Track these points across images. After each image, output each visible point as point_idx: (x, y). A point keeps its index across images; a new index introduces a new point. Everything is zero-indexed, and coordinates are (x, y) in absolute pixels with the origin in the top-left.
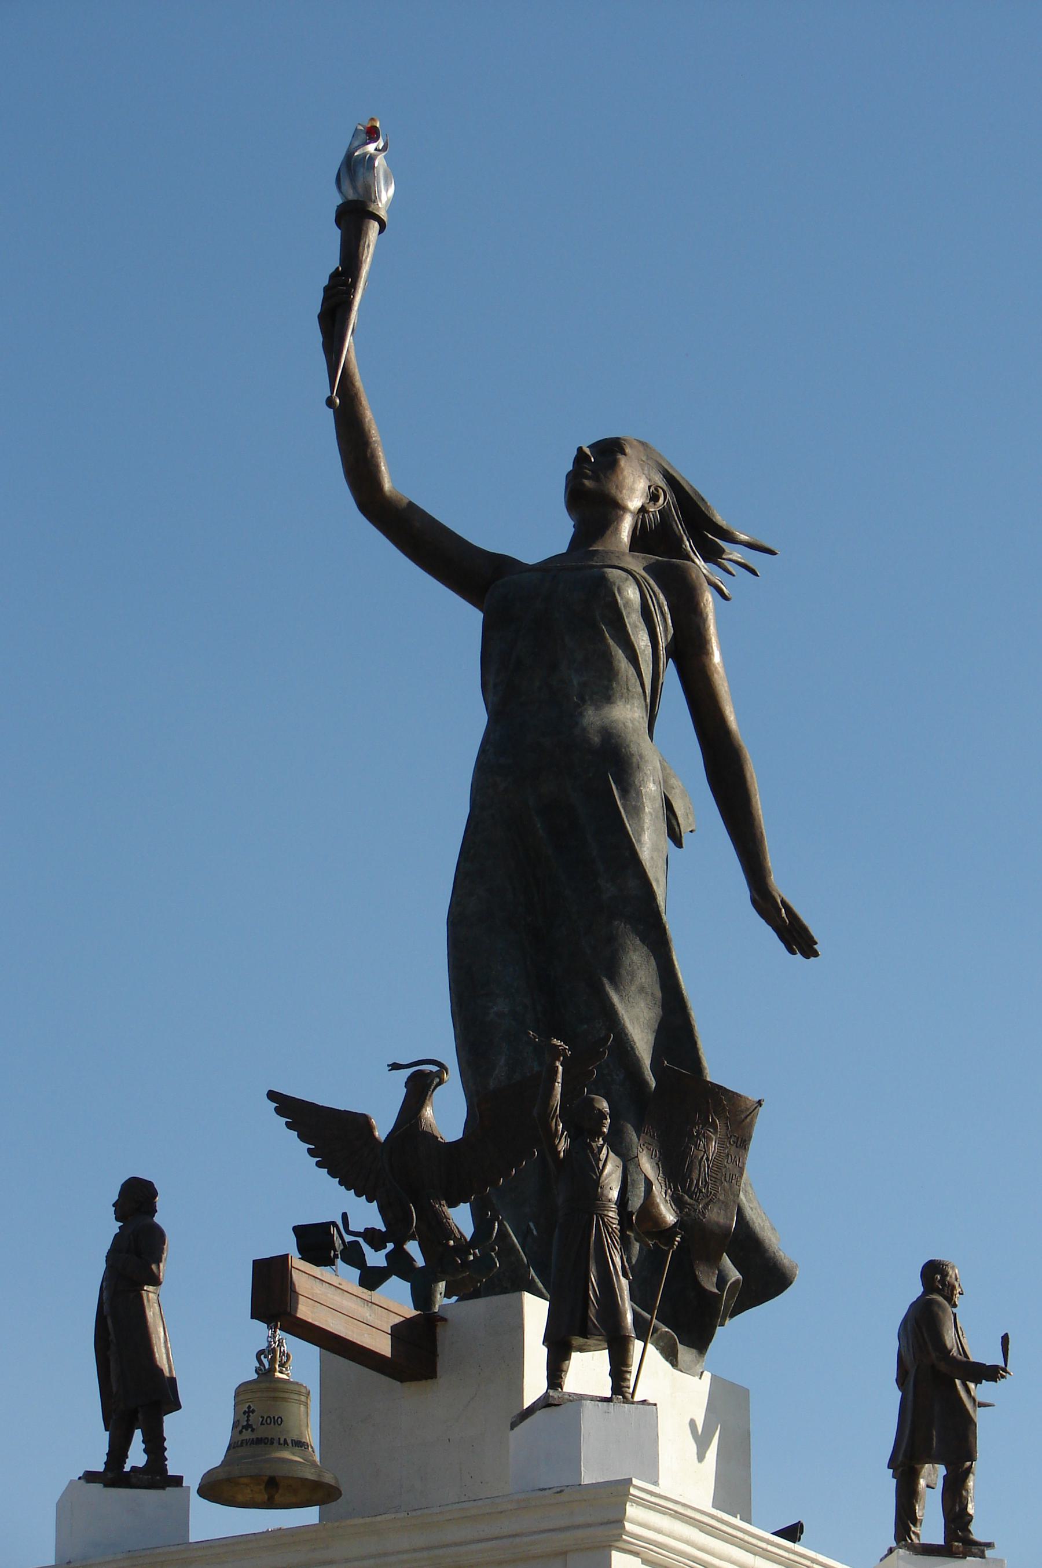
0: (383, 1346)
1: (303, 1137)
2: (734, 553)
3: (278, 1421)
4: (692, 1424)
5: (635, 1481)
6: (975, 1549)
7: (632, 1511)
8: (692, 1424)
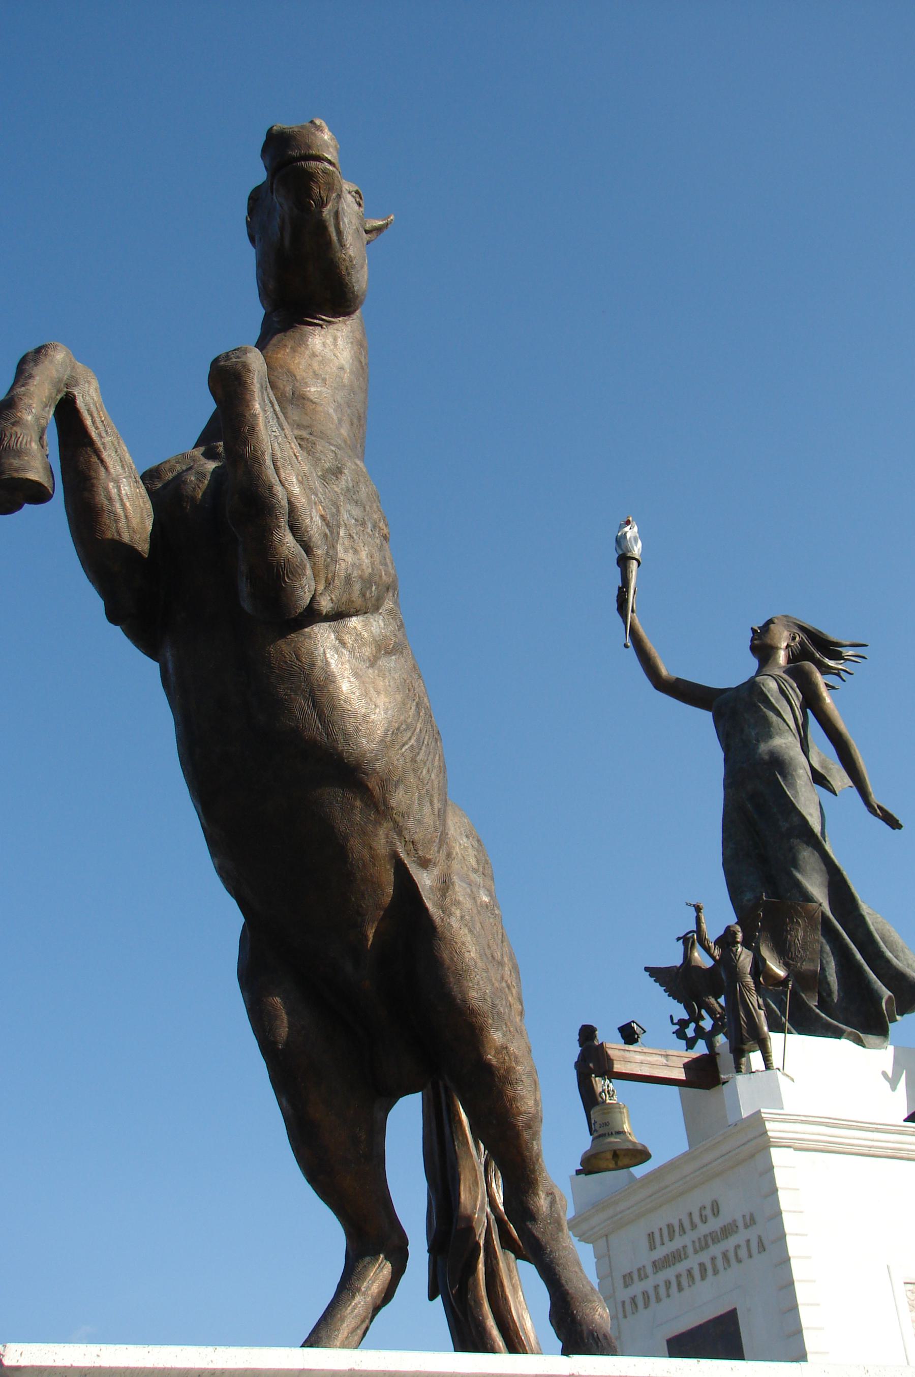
0: (680, 1075)
1: (661, 985)
2: (848, 652)
3: (606, 1124)
4: (884, 1074)
5: (762, 1110)
7: (768, 1126)
8: (884, 1074)
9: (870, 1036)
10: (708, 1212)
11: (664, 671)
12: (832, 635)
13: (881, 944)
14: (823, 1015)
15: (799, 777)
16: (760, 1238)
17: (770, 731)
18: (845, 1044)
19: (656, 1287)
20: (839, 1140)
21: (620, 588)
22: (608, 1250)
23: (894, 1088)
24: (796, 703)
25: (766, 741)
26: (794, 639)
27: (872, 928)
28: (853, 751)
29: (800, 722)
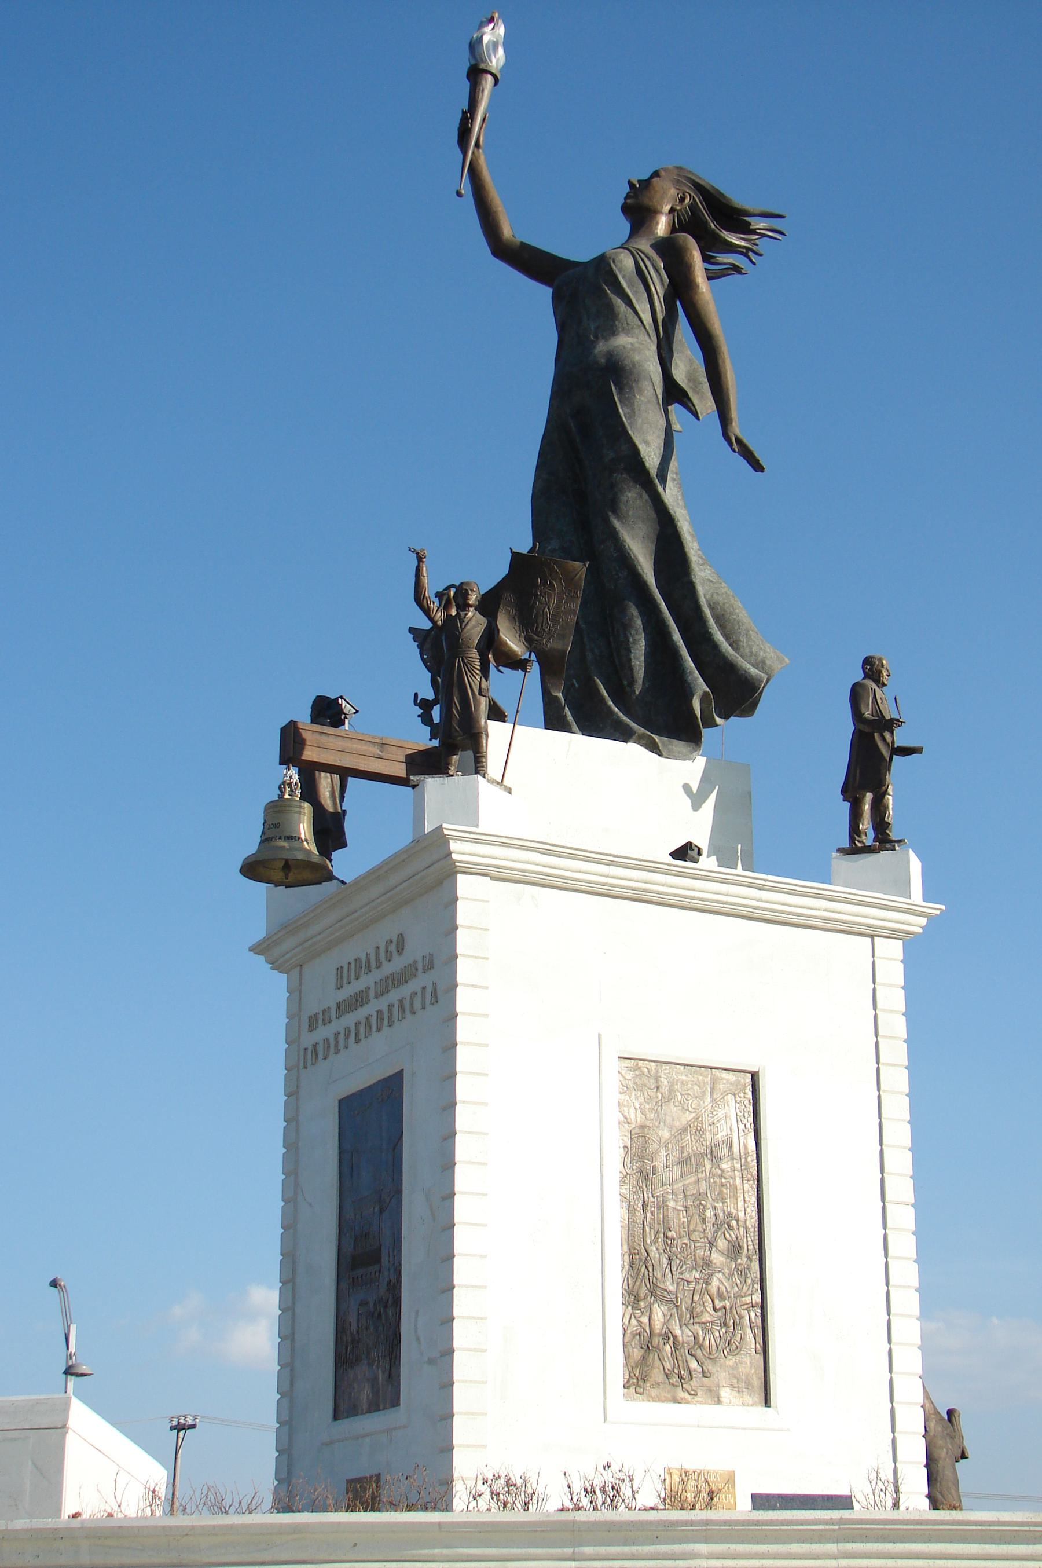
4: (686, 788)
5: (445, 826)
6: (888, 846)
7: (453, 846)
8: (686, 788)
9: (676, 742)
10: (393, 948)
11: (507, 231)
12: (739, 197)
13: (711, 622)
14: (616, 709)
15: (641, 392)
16: (434, 984)
17: (613, 325)
18: (633, 750)
19: (337, 1034)
20: (551, 871)
21: (464, 113)
22: (300, 985)
23: (696, 806)
24: (659, 290)
25: (606, 339)
26: (682, 200)
27: (703, 601)
28: (720, 362)
29: (660, 317)
